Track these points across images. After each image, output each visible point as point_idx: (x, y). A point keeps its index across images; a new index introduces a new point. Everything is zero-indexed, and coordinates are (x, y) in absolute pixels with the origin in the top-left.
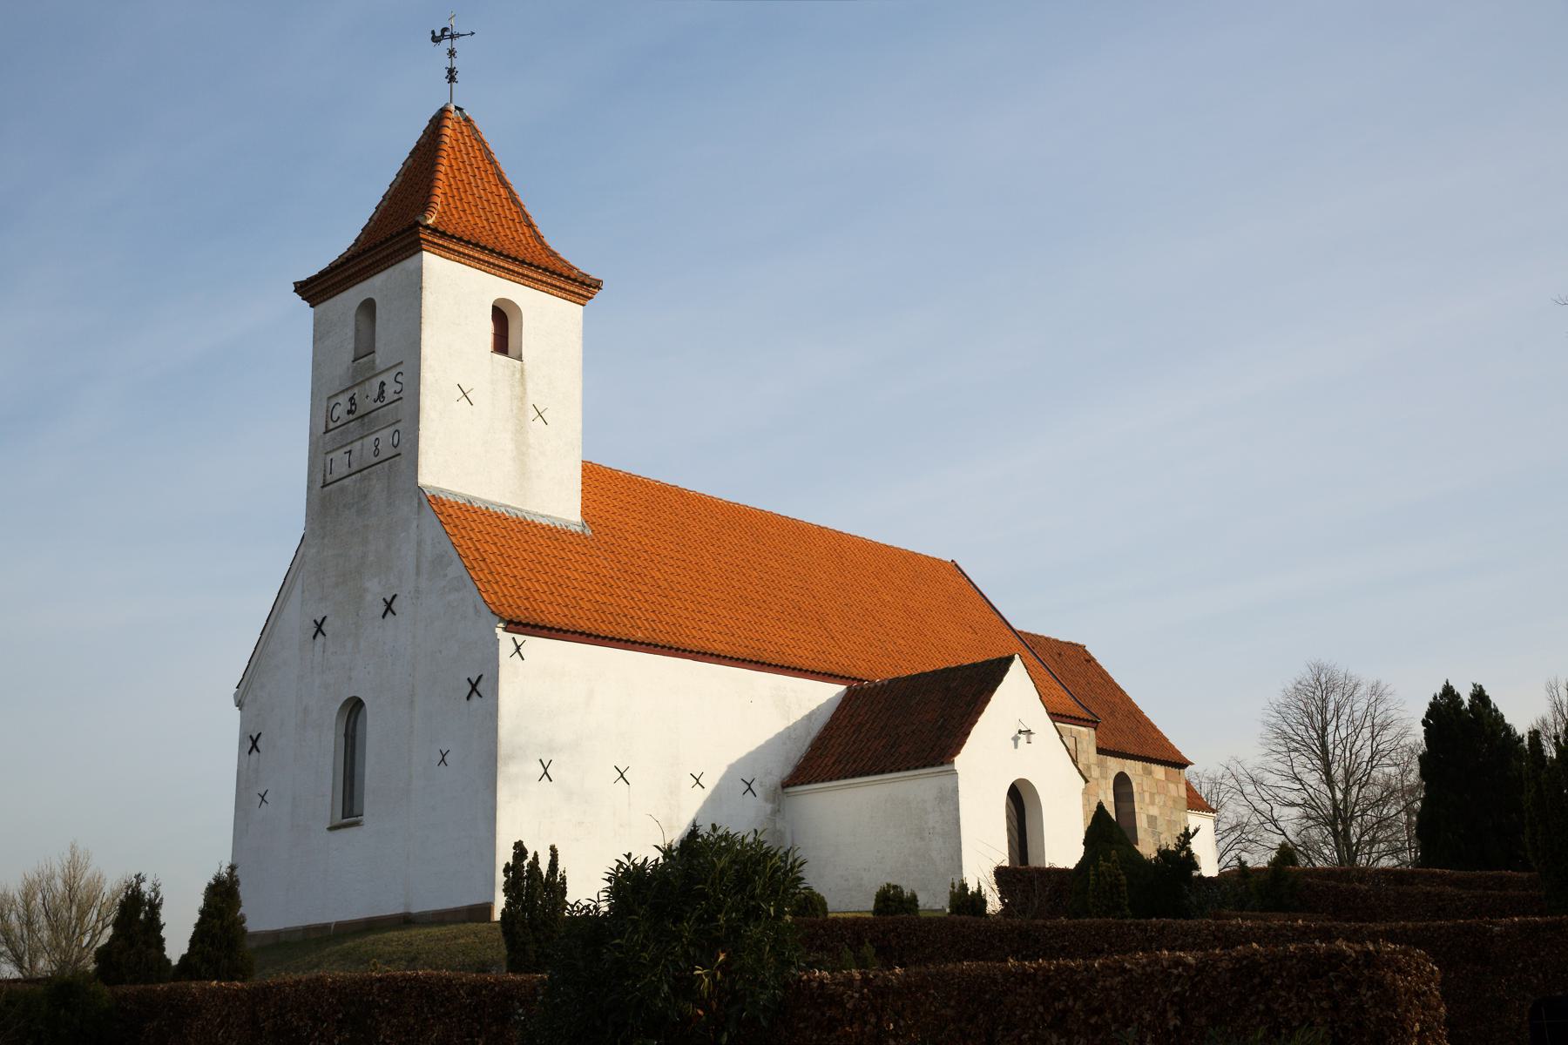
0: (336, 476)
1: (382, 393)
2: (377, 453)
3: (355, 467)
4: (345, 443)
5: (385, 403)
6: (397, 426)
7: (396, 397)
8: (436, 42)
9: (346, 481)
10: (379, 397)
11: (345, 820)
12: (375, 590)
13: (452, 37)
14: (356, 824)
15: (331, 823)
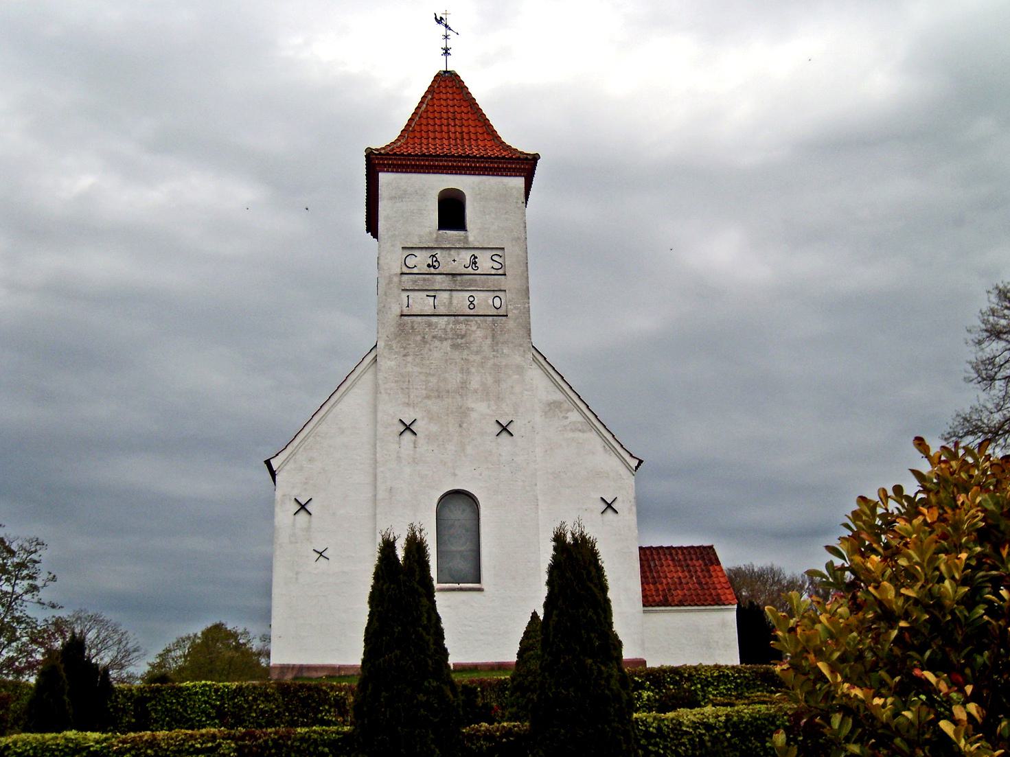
6: (501, 294)
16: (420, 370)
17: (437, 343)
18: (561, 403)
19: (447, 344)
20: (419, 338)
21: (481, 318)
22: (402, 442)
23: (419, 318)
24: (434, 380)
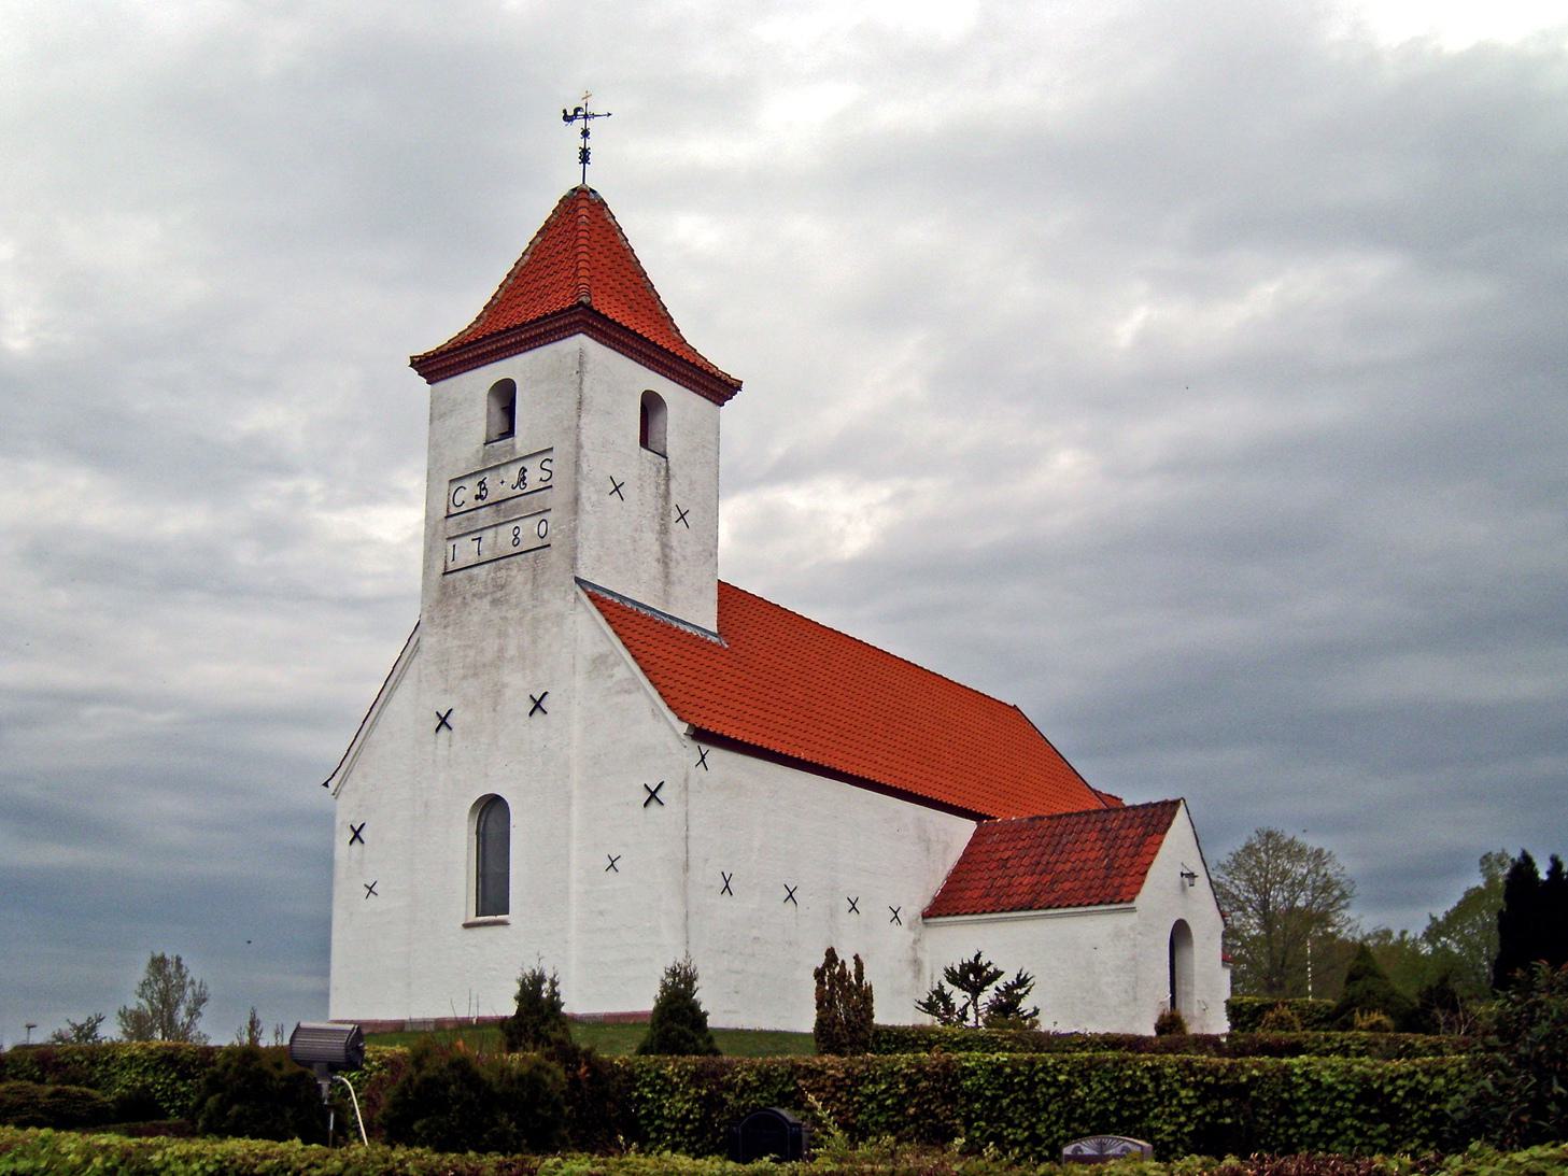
0: (460, 563)
1: (522, 479)
2: (516, 541)
3: (486, 556)
4: (473, 529)
5: (525, 491)
6: (545, 516)
7: (542, 485)
8: (569, 121)
9: (475, 571)
10: (518, 484)
11: (481, 919)
12: (518, 686)
13: (586, 116)
14: (504, 923)
15: (466, 919)
16: (459, 643)
17: (477, 602)
18: (607, 656)
19: (486, 602)
20: (459, 600)
21: (523, 556)
22: (439, 741)
23: (461, 573)
24: (472, 653)
